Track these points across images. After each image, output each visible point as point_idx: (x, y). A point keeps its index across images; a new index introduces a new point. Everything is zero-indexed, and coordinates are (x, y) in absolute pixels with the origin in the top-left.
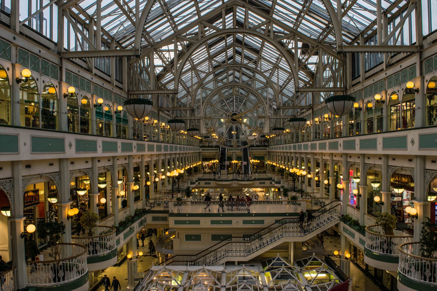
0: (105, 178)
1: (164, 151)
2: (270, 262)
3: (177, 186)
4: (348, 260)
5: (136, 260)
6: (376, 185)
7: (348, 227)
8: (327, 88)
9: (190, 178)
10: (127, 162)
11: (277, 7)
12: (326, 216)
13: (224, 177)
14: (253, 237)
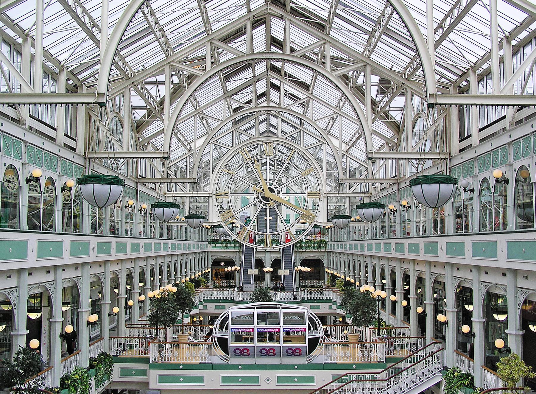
10: (102, 270)
12: (420, 368)
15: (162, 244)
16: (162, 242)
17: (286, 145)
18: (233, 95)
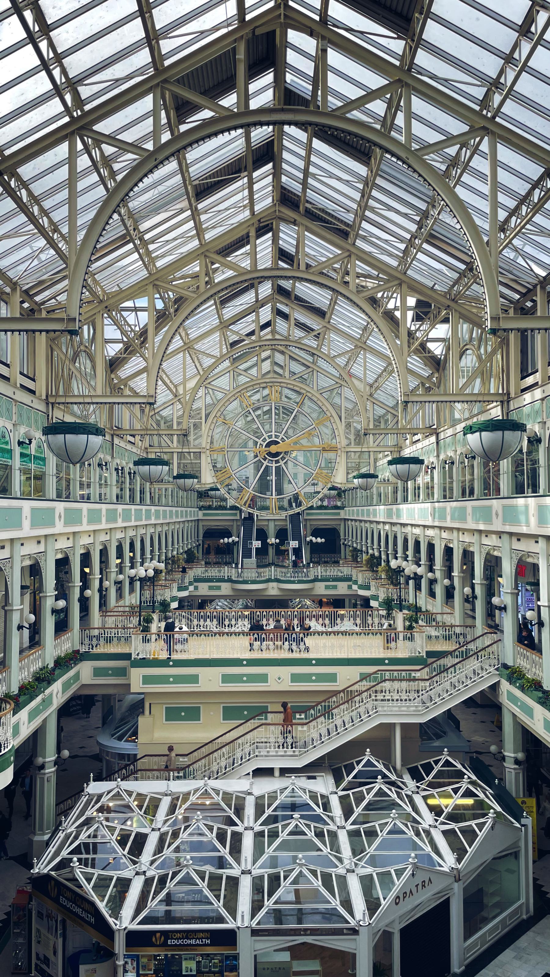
7: (518, 693)
10: (41, 548)
11: (365, 225)
12: (473, 664)
14: (313, 712)
16: (144, 508)
17: (296, 388)
18: (230, 325)
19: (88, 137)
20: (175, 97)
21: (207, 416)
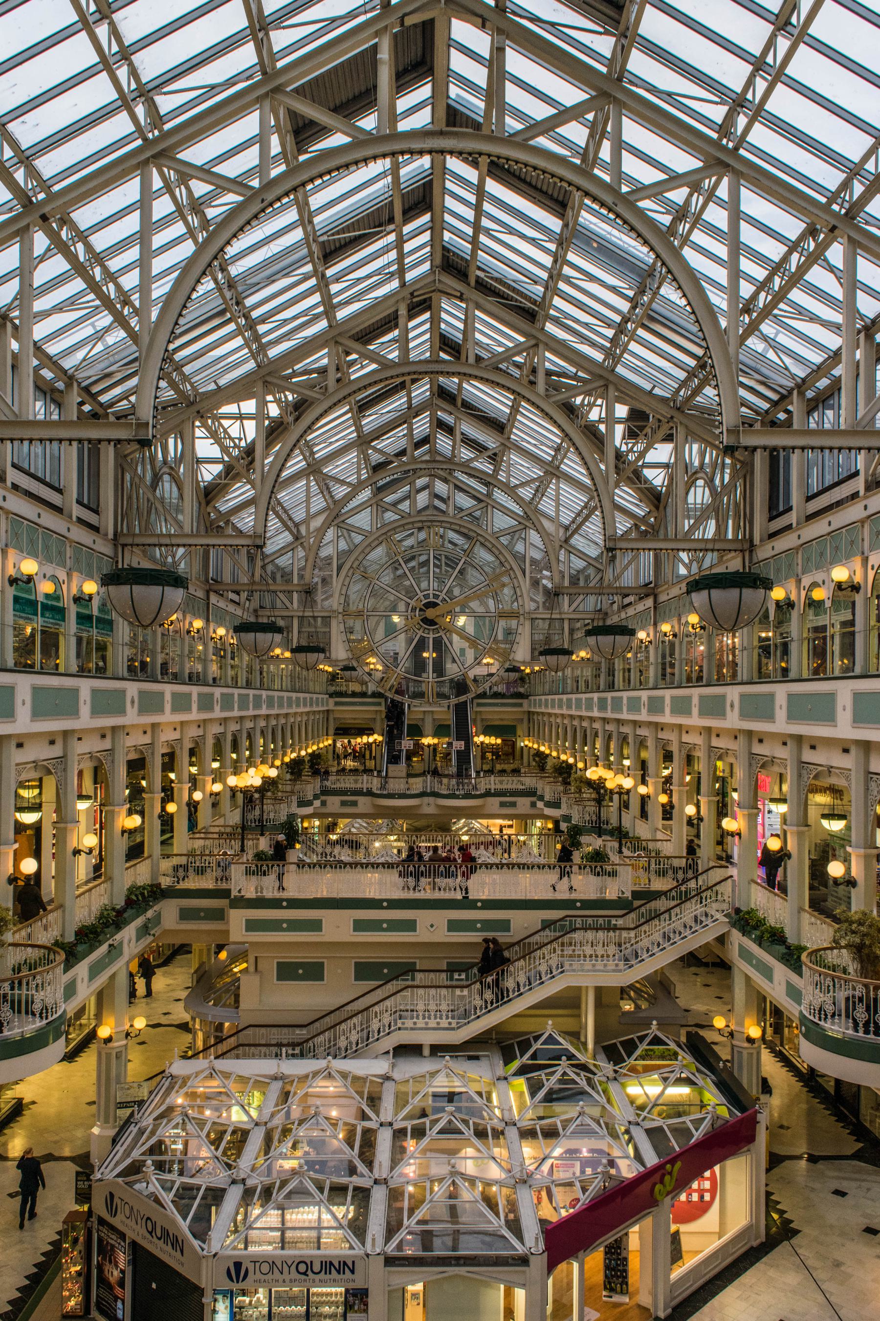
0: (37, 791)
1: (222, 709)
2: (525, 1046)
3: (257, 812)
4: (756, 1045)
5: (124, 1042)
6: (836, 826)
8: (698, 540)
9: (298, 787)
10: (107, 744)
11: (557, 301)
12: (692, 909)
13: (396, 785)
15: (236, 696)
18: (372, 440)
19: (169, 168)
20: (292, 114)
21: (339, 568)
